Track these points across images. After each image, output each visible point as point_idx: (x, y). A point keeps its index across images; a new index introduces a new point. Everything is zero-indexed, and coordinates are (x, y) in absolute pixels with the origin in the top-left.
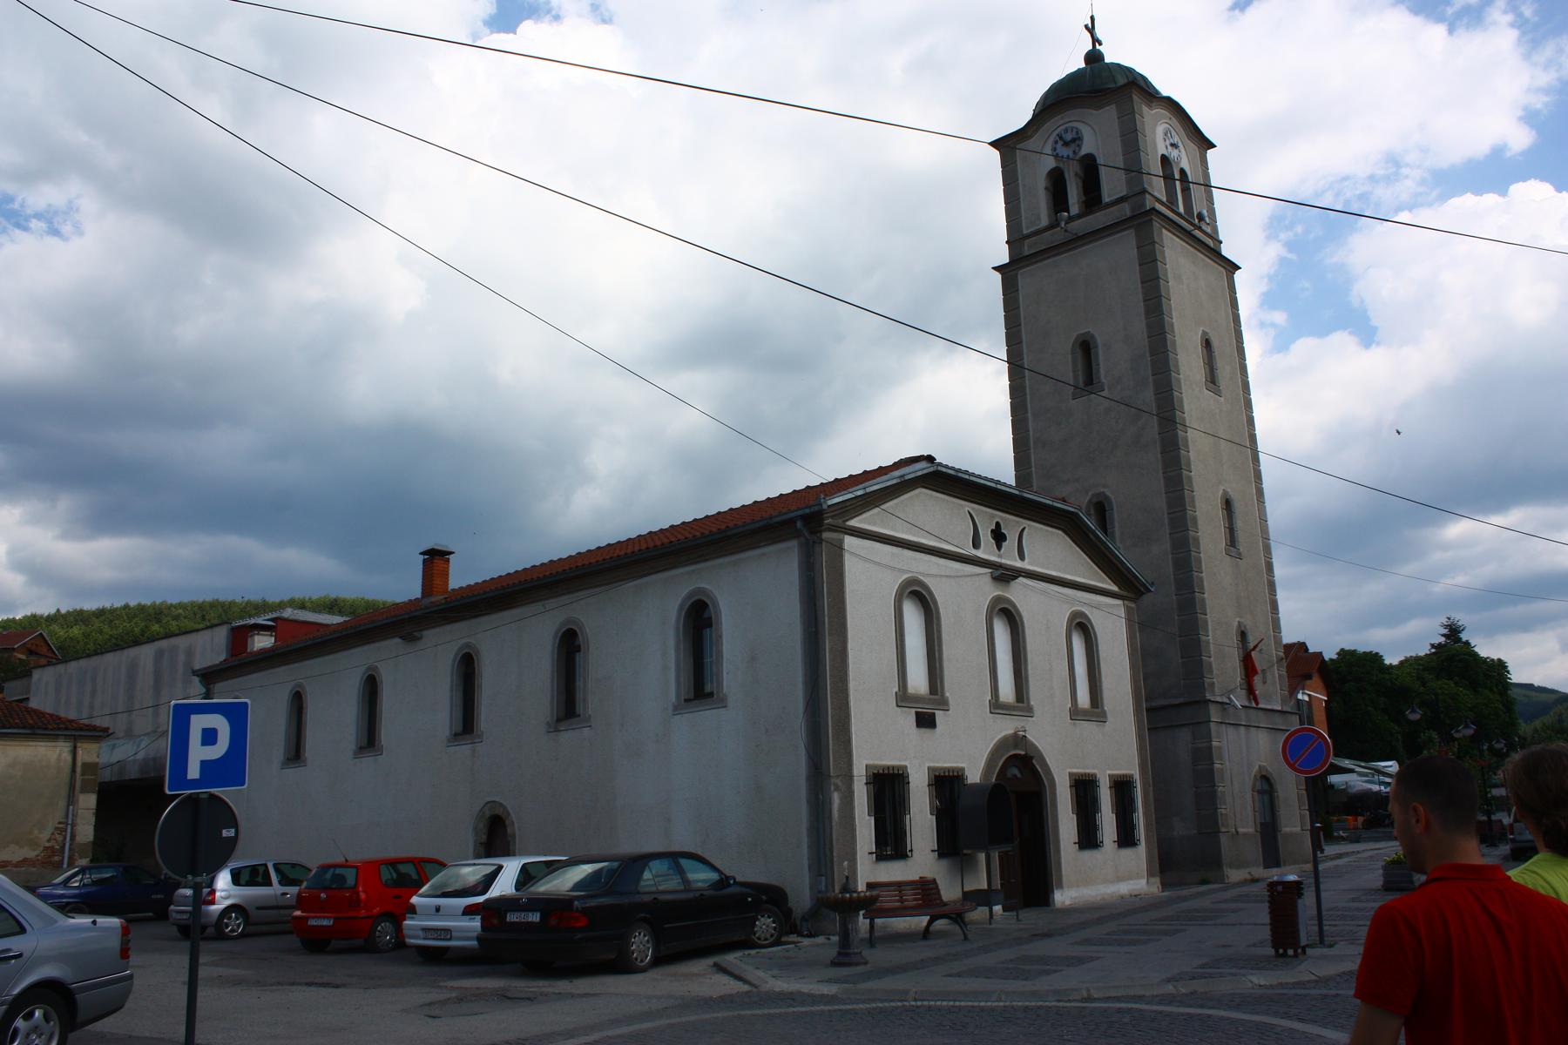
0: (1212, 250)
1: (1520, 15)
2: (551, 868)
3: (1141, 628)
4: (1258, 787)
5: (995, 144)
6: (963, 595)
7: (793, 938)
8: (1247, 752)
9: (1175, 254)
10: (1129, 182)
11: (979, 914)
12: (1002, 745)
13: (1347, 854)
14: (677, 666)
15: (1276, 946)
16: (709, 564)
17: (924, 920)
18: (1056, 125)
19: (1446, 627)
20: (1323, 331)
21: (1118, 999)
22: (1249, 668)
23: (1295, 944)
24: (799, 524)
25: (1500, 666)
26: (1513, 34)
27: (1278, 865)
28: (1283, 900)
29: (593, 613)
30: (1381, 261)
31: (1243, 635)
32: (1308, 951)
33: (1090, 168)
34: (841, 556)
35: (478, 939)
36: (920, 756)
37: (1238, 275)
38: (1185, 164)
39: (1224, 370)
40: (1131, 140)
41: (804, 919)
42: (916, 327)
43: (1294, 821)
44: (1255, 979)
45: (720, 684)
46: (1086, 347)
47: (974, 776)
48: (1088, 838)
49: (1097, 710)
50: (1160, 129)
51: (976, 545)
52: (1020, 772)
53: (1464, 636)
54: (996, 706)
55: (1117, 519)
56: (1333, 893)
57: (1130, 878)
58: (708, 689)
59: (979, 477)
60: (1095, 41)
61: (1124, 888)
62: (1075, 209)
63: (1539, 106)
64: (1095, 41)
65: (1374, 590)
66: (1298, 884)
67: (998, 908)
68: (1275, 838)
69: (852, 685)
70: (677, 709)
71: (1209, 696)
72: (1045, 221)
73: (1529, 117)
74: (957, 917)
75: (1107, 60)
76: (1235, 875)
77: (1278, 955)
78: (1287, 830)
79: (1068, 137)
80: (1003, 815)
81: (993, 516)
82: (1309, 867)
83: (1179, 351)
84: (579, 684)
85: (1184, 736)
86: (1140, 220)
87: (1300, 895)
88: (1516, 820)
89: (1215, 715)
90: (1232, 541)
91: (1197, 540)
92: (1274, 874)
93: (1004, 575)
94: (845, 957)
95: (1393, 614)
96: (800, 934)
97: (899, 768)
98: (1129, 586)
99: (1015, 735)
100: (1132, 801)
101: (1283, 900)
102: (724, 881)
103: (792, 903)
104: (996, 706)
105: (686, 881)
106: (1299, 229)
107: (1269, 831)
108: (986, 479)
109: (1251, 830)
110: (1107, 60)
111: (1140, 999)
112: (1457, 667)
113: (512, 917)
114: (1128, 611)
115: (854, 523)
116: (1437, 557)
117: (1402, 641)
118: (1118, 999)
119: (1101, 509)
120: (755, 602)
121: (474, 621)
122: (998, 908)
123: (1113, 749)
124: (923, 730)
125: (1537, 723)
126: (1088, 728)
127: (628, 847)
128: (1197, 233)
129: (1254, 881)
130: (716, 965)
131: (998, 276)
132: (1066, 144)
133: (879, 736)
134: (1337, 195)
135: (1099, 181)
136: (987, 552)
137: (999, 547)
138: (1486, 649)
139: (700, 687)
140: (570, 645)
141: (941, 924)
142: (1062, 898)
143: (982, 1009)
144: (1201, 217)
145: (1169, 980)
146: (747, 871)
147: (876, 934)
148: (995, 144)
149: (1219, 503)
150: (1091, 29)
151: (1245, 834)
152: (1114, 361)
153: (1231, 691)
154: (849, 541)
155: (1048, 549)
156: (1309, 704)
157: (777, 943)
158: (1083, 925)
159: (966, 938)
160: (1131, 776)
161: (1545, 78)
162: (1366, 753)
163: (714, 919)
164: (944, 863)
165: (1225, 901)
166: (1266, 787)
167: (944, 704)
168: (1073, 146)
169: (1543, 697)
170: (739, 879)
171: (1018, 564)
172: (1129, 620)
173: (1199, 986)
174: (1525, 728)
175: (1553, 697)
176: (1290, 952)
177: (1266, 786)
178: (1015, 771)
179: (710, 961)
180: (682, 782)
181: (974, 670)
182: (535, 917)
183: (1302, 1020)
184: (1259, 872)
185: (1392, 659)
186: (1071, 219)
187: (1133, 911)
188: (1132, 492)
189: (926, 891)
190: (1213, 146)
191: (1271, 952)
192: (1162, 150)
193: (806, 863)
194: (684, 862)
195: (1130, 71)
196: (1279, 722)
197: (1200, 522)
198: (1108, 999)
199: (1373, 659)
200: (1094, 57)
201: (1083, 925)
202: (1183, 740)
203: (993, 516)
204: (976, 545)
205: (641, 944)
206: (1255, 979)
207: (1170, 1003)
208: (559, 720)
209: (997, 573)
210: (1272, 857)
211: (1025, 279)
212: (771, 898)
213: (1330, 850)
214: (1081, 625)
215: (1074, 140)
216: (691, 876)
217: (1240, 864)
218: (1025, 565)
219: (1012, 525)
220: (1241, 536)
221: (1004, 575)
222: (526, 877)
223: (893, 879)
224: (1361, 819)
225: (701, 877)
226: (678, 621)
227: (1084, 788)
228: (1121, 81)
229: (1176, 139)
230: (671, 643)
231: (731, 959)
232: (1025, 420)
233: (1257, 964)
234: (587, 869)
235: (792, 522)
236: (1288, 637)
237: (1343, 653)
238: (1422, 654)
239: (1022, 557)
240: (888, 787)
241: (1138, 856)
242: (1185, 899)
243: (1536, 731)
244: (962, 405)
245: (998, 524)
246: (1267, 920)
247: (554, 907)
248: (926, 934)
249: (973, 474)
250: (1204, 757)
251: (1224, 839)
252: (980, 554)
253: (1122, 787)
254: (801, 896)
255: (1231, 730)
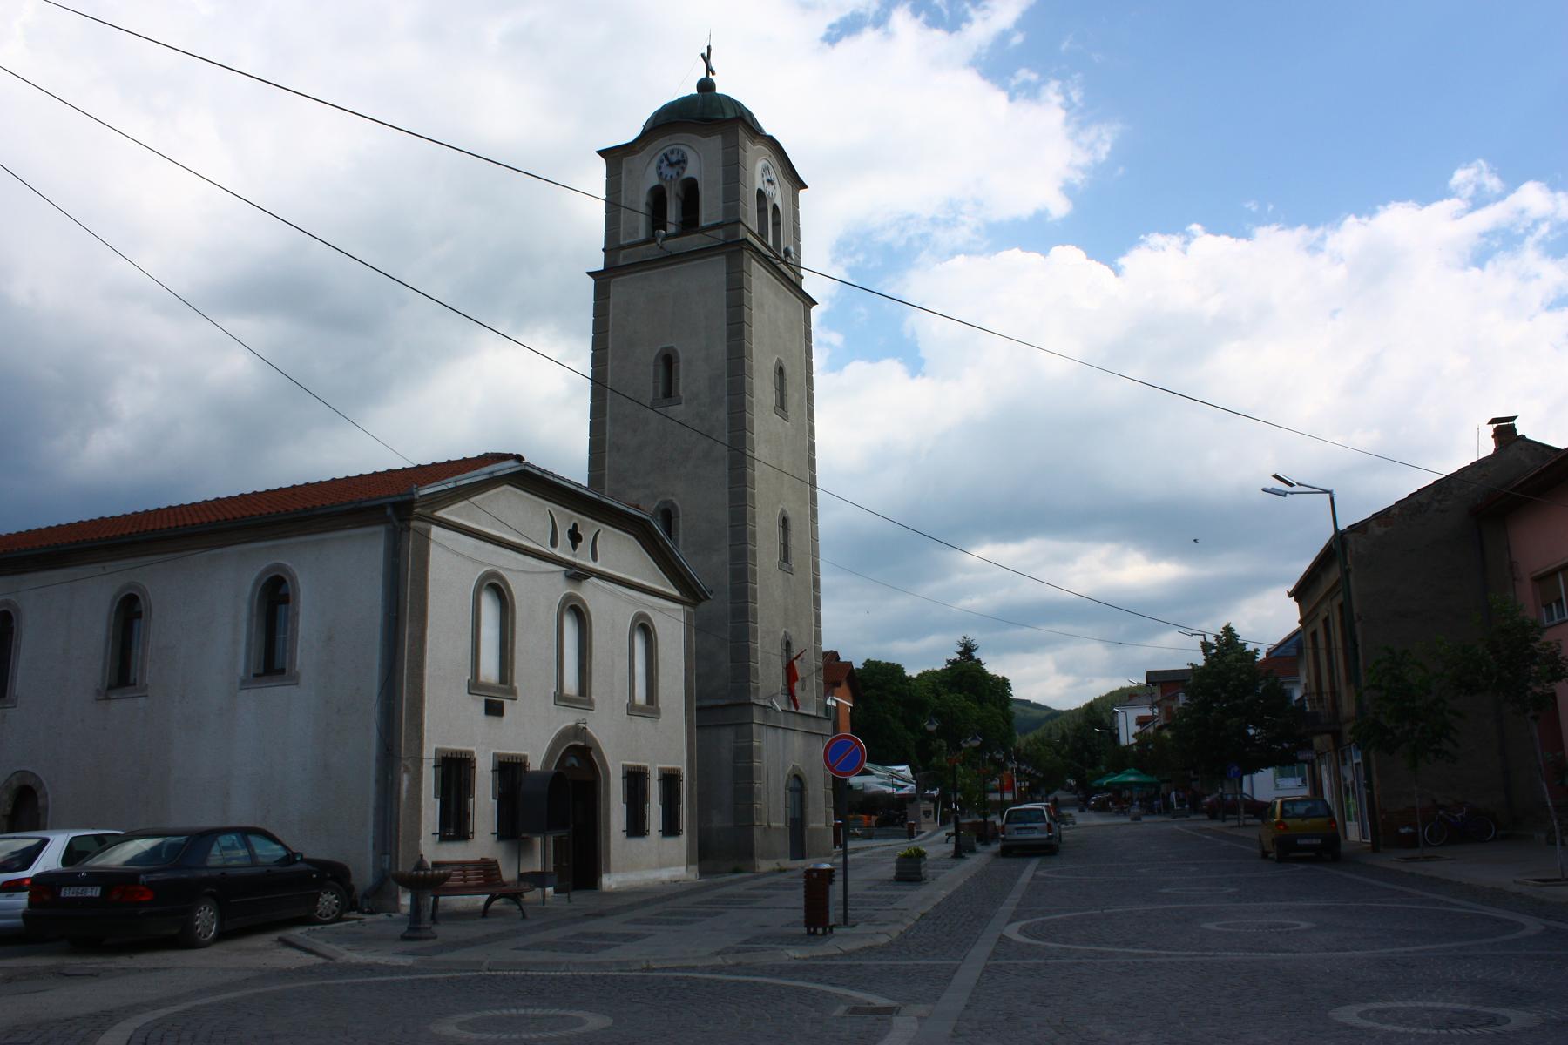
0: (796, 287)
1: (1068, 99)
2: (103, 843)
3: (698, 630)
4: (791, 784)
5: (603, 153)
6: (538, 590)
7: (354, 914)
8: (787, 753)
9: (759, 281)
10: (727, 210)
11: (531, 896)
12: (564, 735)
13: (863, 849)
14: (248, 644)
15: (808, 924)
16: (292, 540)
17: (481, 900)
18: (664, 145)
19: (962, 645)
20: (874, 357)
21: (674, 969)
22: (791, 674)
23: (824, 922)
24: (389, 511)
25: (1004, 683)
26: (1059, 115)
27: (803, 857)
28: (817, 884)
29: (158, 580)
30: (945, 285)
31: (788, 645)
32: (835, 930)
33: (690, 191)
34: (427, 545)
35: (25, 916)
36: (487, 743)
37: (814, 310)
38: (778, 201)
39: (793, 397)
40: (732, 172)
41: (365, 896)
42: (484, 302)
43: (820, 818)
44: (791, 953)
45: (293, 661)
46: (668, 361)
47: (535, 764)
48: (636, 828)
49: (651, 707)
50: (760, 164)
51: (553, 543)
52: (578, 762)
53: (976, 655)
54: (561, 698)
55: (682, 525)
56: (858, 882)
57: (671, 865)
58: (278, 665)
59: (562, 479)
60: (709, 70)
61: (666, 875)
62: (672, 229)
63: (1077, 181)
64: (709, 70)
65: (900, 605)
66: (830, 871)
67: (550, 890)
68: (802, 835)
69: (428, 672)
70: (245, 684)
71: (753, 699)
72: (642, 235)
73: (1068, 190)
74: (515, 897)
75: (718, 91)
76: (764, 865)
77: (809, 933)
78: (812, 825)
79: (674, 158)
80: (560, 802)
81: (571, 517)
82: (840, 860)
83: (755, 375)
84: (136, 651)
85: (727, 736)
86: (732, 247)
87: (831, 881)
88: (1008, 821)
89: (756, 712)
90: (786, 557)
91: (754, 553)
92: (810, 863)
93: (578, 574)
94: (415, 929)
95: (913, 628)
96: (363, 912)
97: (467, 752)
98: (690, 592)
99: (576, 727)
100: (678, 793)
101: (817, 884)
102: (290, 858)
103: (354, 881)
104: (561, 698)
105: (252, 855)
106: (861, 257)
107: (797, 825)
108: (568, 481)
109: (782, 824)
110: (718, 91)
111: (694, 969)
112: (967, 679)
113: (67, 892)
114: (688, 616)
115: (442, 514)
116: (958, 578)
117: (922, 655)
118: (674, 969)
119: (668, 515)
120: (336, 583)
121: (16, 578)
122: (550, 890)
123: (663, 744)
124: (491, 718)
125: (1031, 736)
126: (643, 723)
127: (207, 820)
128: (783, 267)
129: (782, 871)
130: (280, 940)
131: (591, 281)
132: (671, 165)
133: (449, 721)
134: (902, 231)
135: (695, 206)
136: (563, 551)
137: (574, 547)
138: (993, 667)
139: (271, 662)
140: (129, 611)
141: (498, 904)
142: (609, 882)
143: (553, 978)
144: (787, 253)
145: (718, 954)
146: (315, 850)
147: (440, 911)
148: (603, 153)
149: (776, 520)
150: (706, 59)
151: (777, 829)
152: (694, 377)
153: (773, 696)
154: (436, 532)
155: (619, 553)
156: (836, 709)
157: (339, 919)
158: (631, 907)
159: (524, 916)
160: (678, 770)
161: (1083, 159)
162: (882, 759)
163: (280, 894)
164: (502, 845)
165: (758, 888)
166: (798, 785)
167: (512, 694)
168: (677, 168)
169: (1037, 713)
170: (306, 856)
171: (591, 564)
172: (688, 624)
173: (743, 958)
174: (1021, 740)
175: (1045, 713)
176: (820, 931)
177: (798, 785)
178: (574, 761)
179: (275, 936)
180: (244, 756)
181: (540, 661)
182: (95, 892)
183: (833, 985)
184: (787, 863)
185: (912, 672)
186: (668, 237)
187: (673, 896)
188: (698, 503)
189: (488, 869)
190: (805, 187)
191: (804, 930)
192: (759, 183)
193: (370, 842)
194: (253, 839)
195: (737, 105)
196: (813, 726)
197: (758, 537)
198: (664, 969)
199: (895, 671)
200: (706, 86)
201: (631, 907)
202: (726, 739)
203: (571, 517)
204: (553, 543)
205: (205, 919)
206: (791, 953)
207: (719, 973)
208: (110, 688)
209: (572, 572)
210: (798, 851)
211: (617, 288)
212: (333, 875)
213: (851, 845)
214: (644, 627)
215: (678, 162)
216: (258, 851)
217: (770, 855)
218: (597, 566)
219: (588, 526)
220: (793, 553)
221: (578, 574)
222: (73, 854)
223: (460, 859)
224: (874, 818)
225: (268, 852)
226: (252, 595)
227: (635, 779)
228: (730, 115)
229: (773, 176)
230: (244, 614)
231: (297, 933)
232: (604, 423)
233: (791, 940)
234: (146, 844)
235: (382, 507)
236: (826, 646)
237: (868, 663)
238: (938, 668)
239: (595, 558)
240: (455, 769)
241: (680, 845)
242: (723, 885)
243: (1028, 743)
244: (530, 390)
245: (575, 525)
246: (802, 903)
247: (107, 879)
248: (485, 912)
249: (557, 476)
250: (744, 756)
251: (757, 833)
252: (557, 552)
253: (670, 780)
254: (364, 874)
255: (771, 732)
